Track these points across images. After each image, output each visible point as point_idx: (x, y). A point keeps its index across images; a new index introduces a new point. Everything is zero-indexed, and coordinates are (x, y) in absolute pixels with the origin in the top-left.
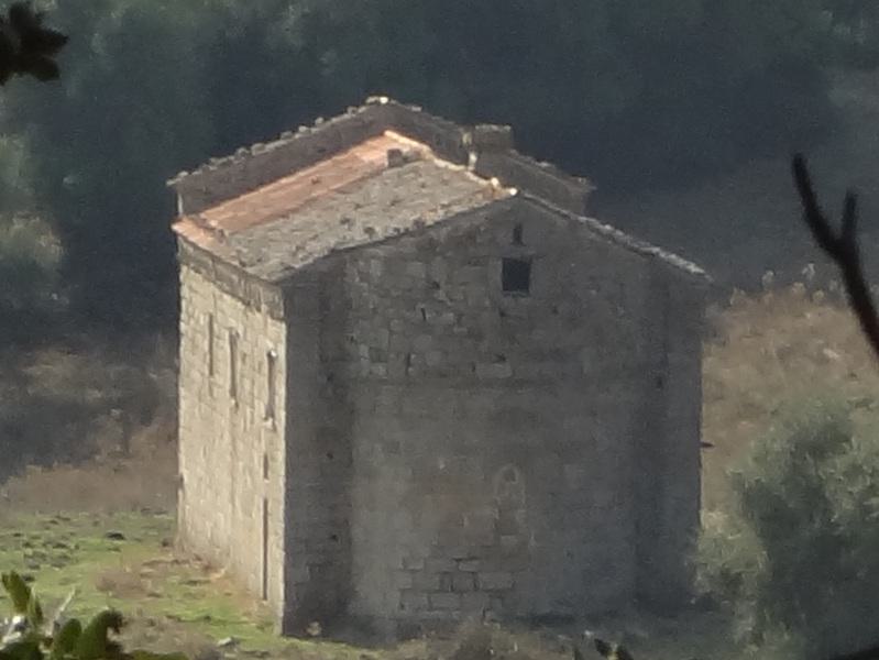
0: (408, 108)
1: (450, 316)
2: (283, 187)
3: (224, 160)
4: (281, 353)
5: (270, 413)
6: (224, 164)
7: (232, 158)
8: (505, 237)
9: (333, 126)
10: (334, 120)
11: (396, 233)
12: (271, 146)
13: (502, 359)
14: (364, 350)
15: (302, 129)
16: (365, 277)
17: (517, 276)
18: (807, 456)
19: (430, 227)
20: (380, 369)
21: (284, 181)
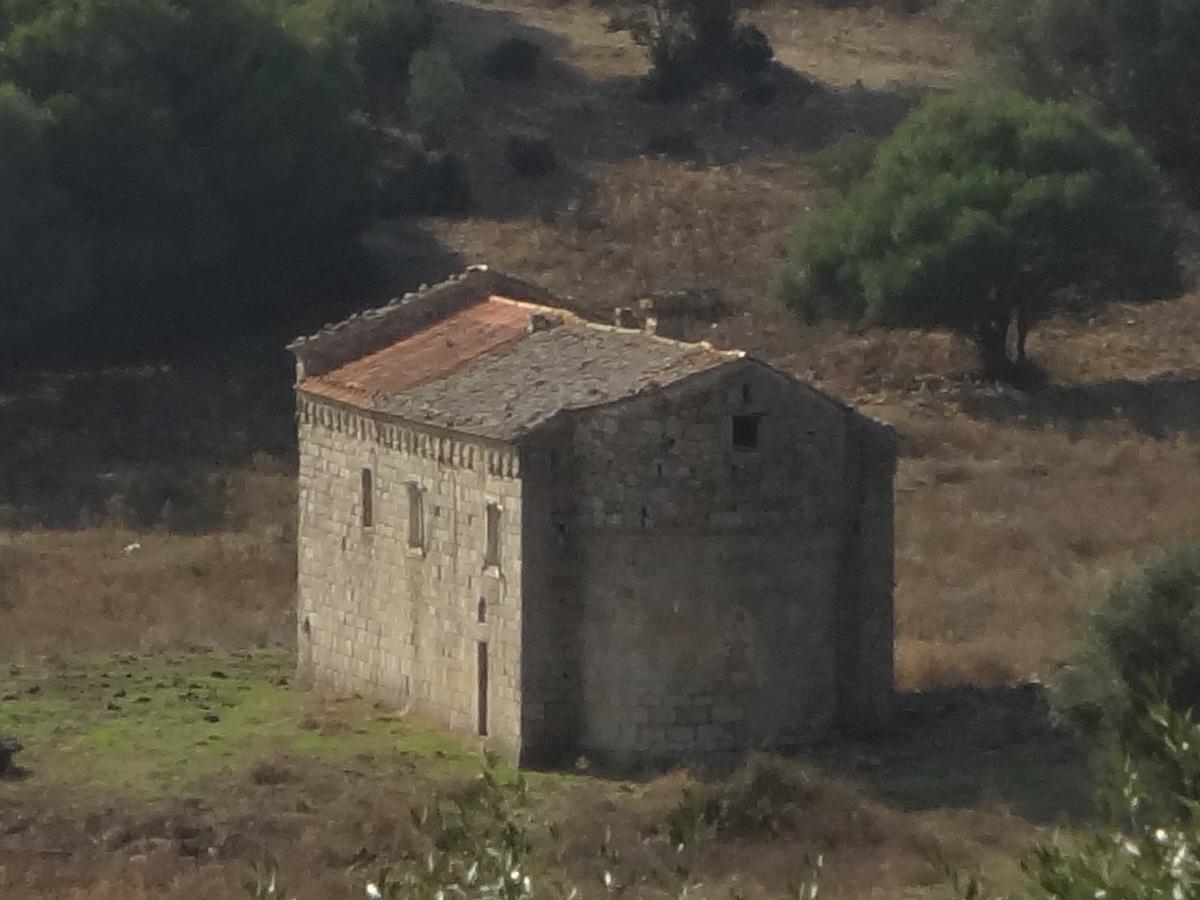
1: (684, 471)
2: (405, 351)
3: (340, 325)
4: (514, 506)
5: (492, 559)
6: (339, 330)
7: (345, 323)
8: (734, 396)
9: (439, 292)
10: (440, 286)
11: (630, 395)
12: (381, 312)
13: (733, 508)
14: (598, 504)
15: (408, 295)
16: (600, 435)
17: (745, 431)
19: (663, 388)
21: (401, 344)
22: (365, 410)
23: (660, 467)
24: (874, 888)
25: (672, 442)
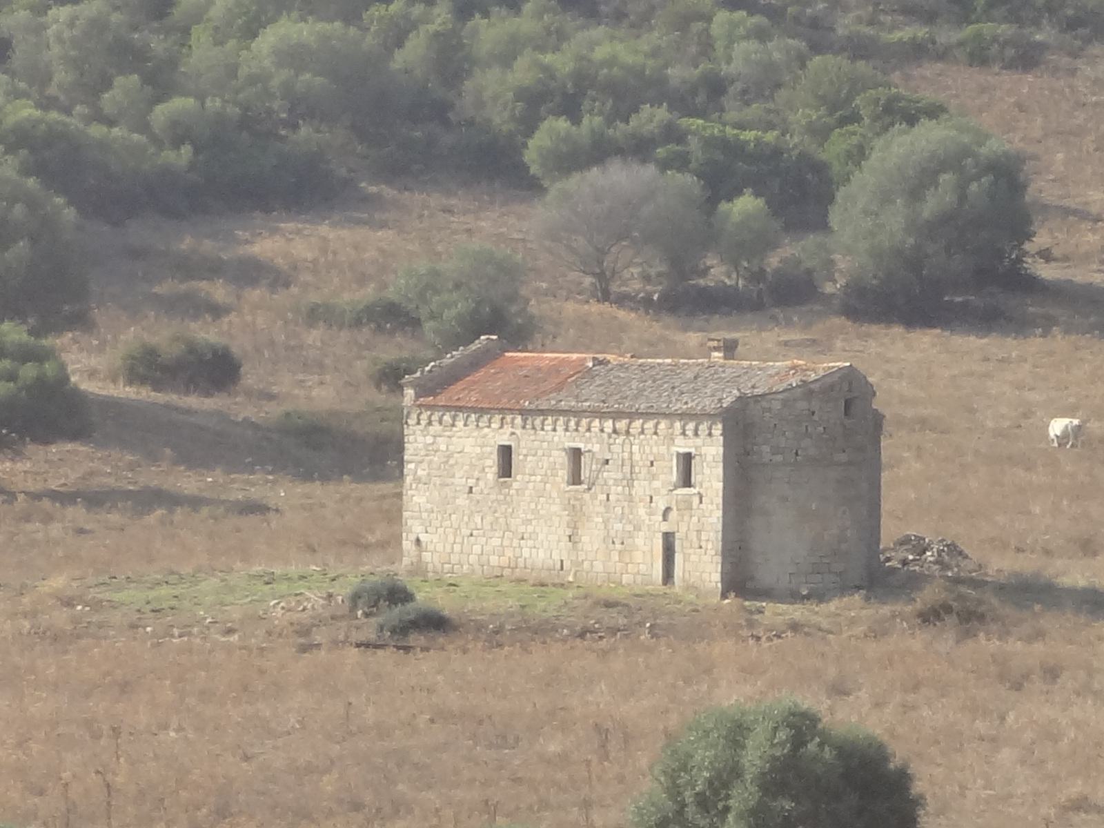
0: (277, 225)
1: (821, 429)
14: (766, 449)
18: (65, 658)
20: (779, 458)
22: (469, 408)
23: (807, 427)
24: (182, 147)
25: (813, 413)
